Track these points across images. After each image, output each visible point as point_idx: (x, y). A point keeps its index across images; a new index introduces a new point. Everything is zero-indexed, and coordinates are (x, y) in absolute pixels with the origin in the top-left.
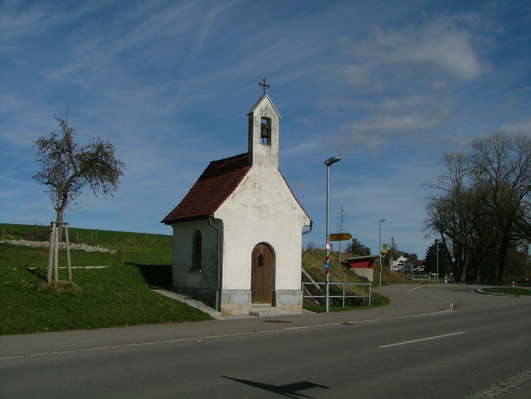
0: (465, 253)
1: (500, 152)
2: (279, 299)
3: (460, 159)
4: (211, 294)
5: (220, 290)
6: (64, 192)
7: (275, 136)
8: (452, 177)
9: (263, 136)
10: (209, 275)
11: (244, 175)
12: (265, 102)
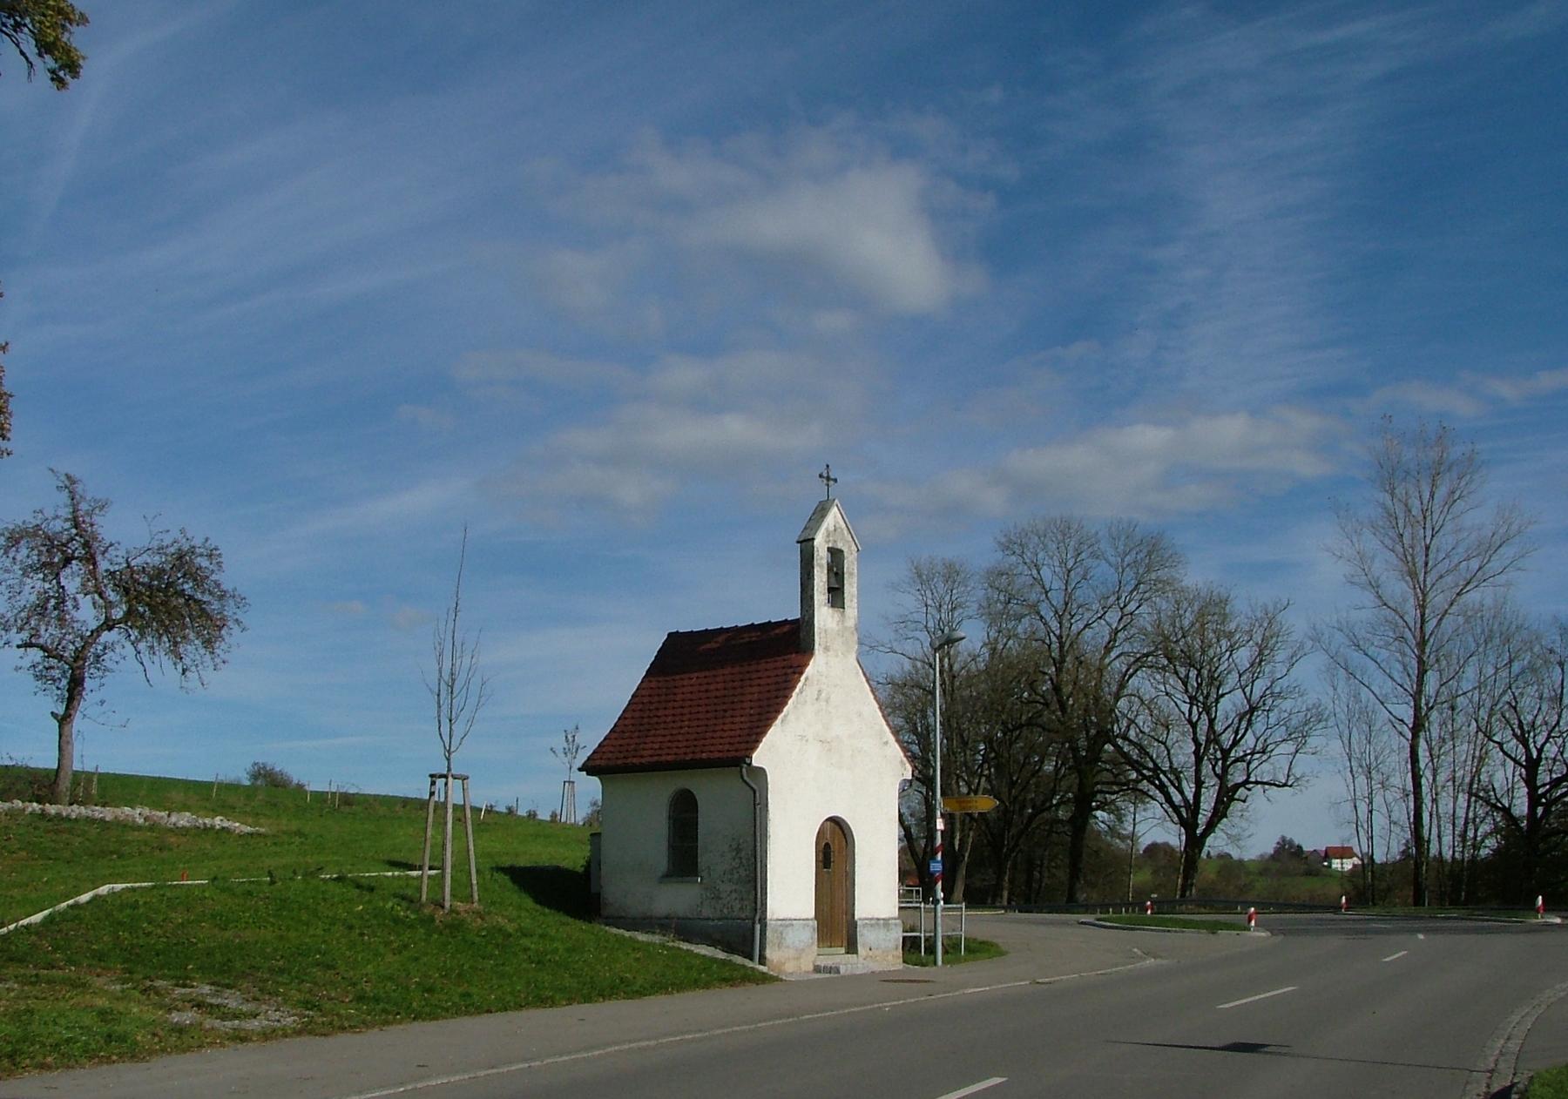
0: (962, 831)
1: (1070, 564)
2: (865, 937)
3: (952, 574)
4: (741, 931)
5: (763, 920)
6: (72, 676)
7: (851, 589)
8: (931, 624)
9: (830, 590)
10: (726, 888)
11: (801, 673)
12: (833, 517)
